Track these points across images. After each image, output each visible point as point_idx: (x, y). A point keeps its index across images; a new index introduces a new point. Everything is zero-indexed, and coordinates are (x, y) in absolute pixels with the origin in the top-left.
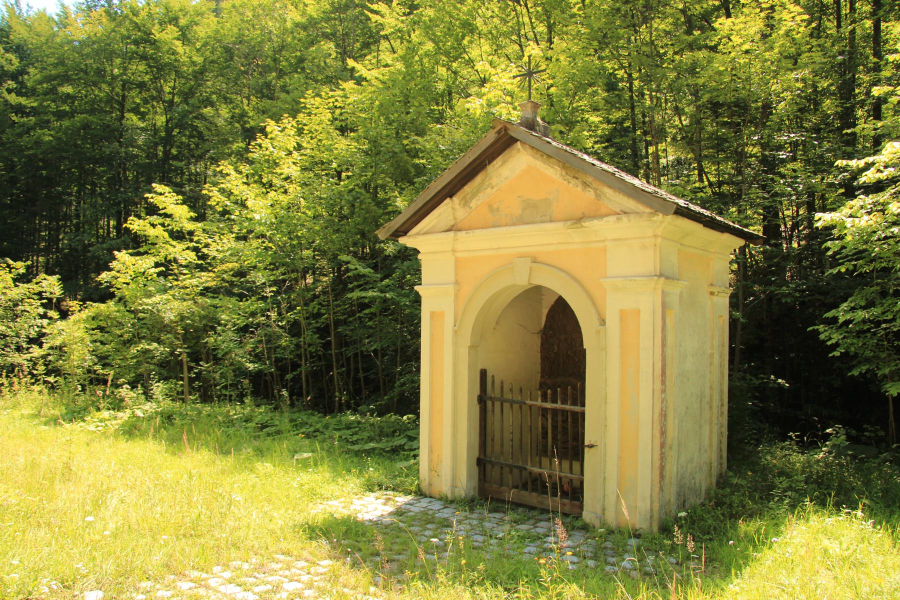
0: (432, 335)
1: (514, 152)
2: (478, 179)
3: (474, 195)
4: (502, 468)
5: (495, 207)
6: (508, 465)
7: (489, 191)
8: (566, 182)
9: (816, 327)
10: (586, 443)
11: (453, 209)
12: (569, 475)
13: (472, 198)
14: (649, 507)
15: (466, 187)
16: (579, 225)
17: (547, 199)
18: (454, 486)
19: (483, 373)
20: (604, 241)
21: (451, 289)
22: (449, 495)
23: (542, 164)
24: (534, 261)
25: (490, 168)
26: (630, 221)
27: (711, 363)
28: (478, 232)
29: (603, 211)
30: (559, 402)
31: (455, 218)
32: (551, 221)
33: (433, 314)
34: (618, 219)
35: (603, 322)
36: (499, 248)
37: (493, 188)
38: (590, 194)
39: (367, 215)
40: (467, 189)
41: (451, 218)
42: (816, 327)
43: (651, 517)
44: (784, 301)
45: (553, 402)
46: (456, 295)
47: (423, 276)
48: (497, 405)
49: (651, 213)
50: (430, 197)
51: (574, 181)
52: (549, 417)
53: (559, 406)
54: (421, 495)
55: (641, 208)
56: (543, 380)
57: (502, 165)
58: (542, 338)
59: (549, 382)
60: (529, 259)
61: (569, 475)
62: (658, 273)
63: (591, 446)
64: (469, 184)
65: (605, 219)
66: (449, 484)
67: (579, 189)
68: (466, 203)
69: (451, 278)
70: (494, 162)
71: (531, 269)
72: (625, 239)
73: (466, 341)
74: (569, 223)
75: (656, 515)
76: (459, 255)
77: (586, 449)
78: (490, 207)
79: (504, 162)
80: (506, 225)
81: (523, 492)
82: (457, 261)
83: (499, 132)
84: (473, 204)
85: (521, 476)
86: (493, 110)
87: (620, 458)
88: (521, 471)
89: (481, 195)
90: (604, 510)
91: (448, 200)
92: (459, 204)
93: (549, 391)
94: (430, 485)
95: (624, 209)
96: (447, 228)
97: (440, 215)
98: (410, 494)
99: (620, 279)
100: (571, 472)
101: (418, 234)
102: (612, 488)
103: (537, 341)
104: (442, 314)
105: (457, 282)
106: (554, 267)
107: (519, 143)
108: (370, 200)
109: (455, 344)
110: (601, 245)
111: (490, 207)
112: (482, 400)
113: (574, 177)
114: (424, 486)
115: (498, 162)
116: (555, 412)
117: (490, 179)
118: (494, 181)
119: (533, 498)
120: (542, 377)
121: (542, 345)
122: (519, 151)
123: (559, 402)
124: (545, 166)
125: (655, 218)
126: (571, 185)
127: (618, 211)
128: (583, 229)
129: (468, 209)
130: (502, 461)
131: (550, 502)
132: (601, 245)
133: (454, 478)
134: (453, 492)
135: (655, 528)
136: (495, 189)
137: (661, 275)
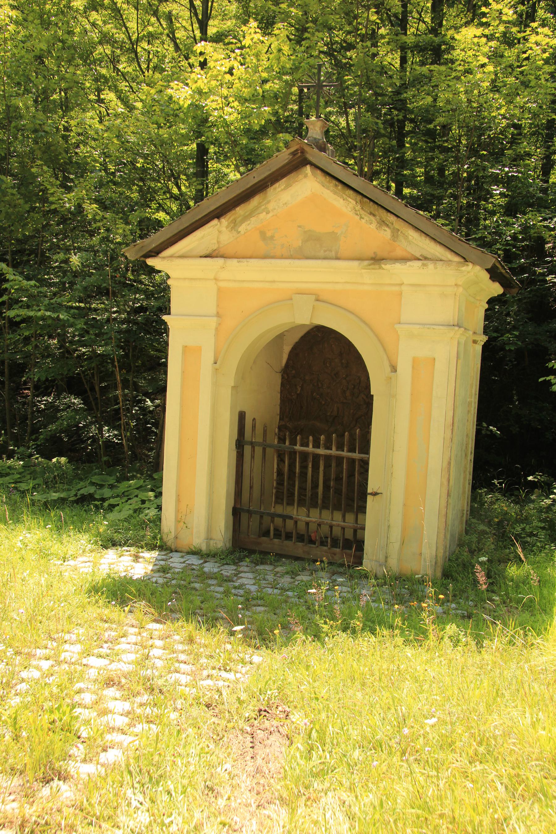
0: (183, 372)
1: (301, 177)
2: (255, 201)
3: (246, 218)
4: (261, 517)
5: (269, 234)
6: (269, 514)
7: (263, 215)
8: (358, 218)
9: (548, 378)
10: (369, 491)
11: (220, 232)
12: (343, 524)
13: (242, 221)
14: (434, 553)
15: (238, 209)
16: (377, 267)
17: (333, 232)
18: (209, 539)
19: (242, 416)
20: (402, 284)
21: (213, 322)
22: (204, 548)
23: (331, 194)
24: (317, 300)
25: (271, 191)
26: (436, 268)
27: (469, 411)
28: (254, 262)
29: (399, 253)
30: (334, 448)
31: (218, 242)
32: (337, 258)
33: (185, 349)
34: (424, 265)
35: (394, 369)
36: (274, 282)
37: (268, 213)
38: (387, 233)
39: (11, 210)
40: (240, 211)
41: (215, 241)
42: (548, 378)
43: (436, 563)
44: (507, 348)
45: (338, 449)
46: (217, 329)
47: (172, 305)
48: (259, 450)
49: (459, 263)
50: (200, 217)
51: (367, 217)
52: (333, 465)
53: (334, 452)
54: (166, 549)
55: (449, 255)
56: (283, 423)
57: (285, 189)
58: (283, 378)
59: (289, 425)
60: (313, 297)
61: (343, 524)
62: (456, 323)
63: (375, 494)
64: (242, 205)
65: (409, 263)
66: (203, 535)
67: (373, 226)
68: (234, 226)
69: (213, 310)
70: (277, 185)
71: (314, 308)
72: (424, 286)
73: (230, 380)
74: (366, 263)
75: (440, 562)
76: (222, 284)
77: (369, 498)
78: (263, 234)
79: (288, 186)
80: (282, 257)
81: (287, 543)
82: (220, 290)
83: (294, 154)
84: (242, 228)
85: (261, 523)
86: (203, 103)
87: (404, 505)
88: (284, 521)
89: (253, 219)
90: (386, 557)
91: (215, 221)
92: (227, 227)
93: (322, 437)
94: (176, 537)
95: (425, 254)
96: (207, 252)
97: (202, 238)
98: (153, 549)
99: (418, 326)
100: (344, 521)
101: (171, 256)
102: (396, 535)
103: (278, 380)
104: (199, 349)
105: (218, 315)
106: (336, 305)
107: (308, 167)
108: (15, 191)
109: (216, 385)
110: (397, 288)
111: (263, 234)
112: (240, 444)
113: (371, 214)
114: (169, 539)
115: (281, 184)
116: (328, 458)
117: (269, 202)
118: (271, 206)
119: (299, 549)
120: (281, 419)
121: (282, 385)
122: (306, 176)
123: (334, 448)
124: (336, 197)
125: (464, 269)
126: (363, 221)
127: (418, 255)
128: (381, 271)
129: (234, 233)
130: (262, 510)
131: (317, 551)
132: (397, 288)
133: (209, 530)
134: (208, 545)
135: (439, 574)
136: (271, 215)
137: (459, 326)
